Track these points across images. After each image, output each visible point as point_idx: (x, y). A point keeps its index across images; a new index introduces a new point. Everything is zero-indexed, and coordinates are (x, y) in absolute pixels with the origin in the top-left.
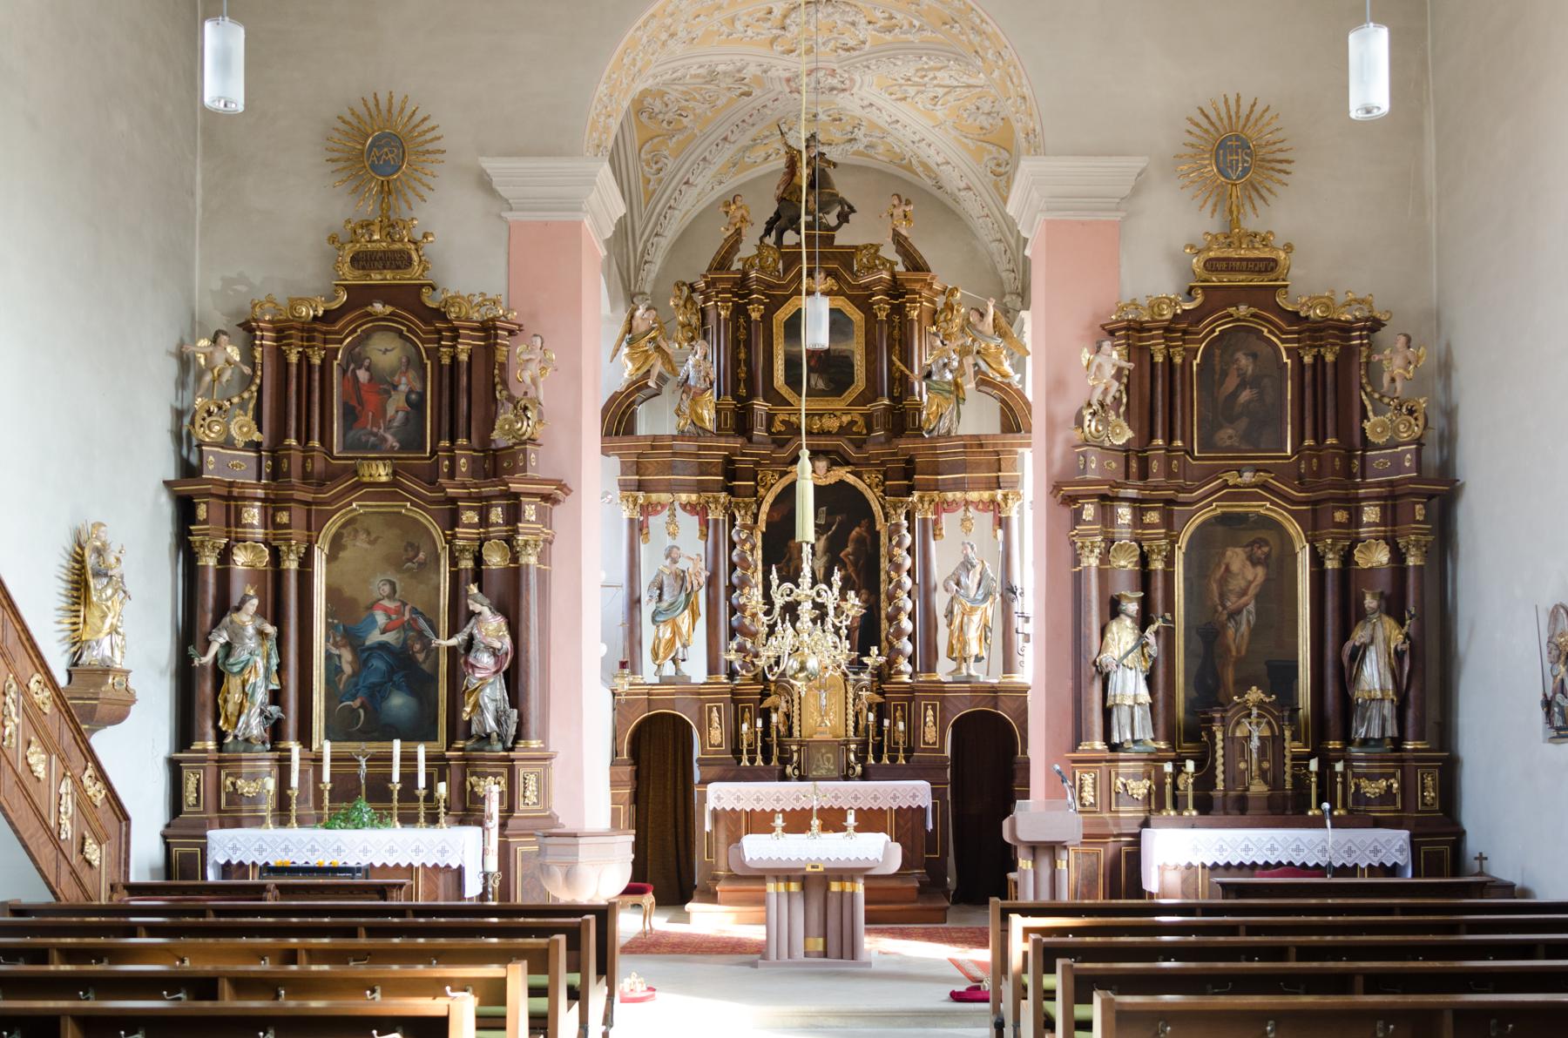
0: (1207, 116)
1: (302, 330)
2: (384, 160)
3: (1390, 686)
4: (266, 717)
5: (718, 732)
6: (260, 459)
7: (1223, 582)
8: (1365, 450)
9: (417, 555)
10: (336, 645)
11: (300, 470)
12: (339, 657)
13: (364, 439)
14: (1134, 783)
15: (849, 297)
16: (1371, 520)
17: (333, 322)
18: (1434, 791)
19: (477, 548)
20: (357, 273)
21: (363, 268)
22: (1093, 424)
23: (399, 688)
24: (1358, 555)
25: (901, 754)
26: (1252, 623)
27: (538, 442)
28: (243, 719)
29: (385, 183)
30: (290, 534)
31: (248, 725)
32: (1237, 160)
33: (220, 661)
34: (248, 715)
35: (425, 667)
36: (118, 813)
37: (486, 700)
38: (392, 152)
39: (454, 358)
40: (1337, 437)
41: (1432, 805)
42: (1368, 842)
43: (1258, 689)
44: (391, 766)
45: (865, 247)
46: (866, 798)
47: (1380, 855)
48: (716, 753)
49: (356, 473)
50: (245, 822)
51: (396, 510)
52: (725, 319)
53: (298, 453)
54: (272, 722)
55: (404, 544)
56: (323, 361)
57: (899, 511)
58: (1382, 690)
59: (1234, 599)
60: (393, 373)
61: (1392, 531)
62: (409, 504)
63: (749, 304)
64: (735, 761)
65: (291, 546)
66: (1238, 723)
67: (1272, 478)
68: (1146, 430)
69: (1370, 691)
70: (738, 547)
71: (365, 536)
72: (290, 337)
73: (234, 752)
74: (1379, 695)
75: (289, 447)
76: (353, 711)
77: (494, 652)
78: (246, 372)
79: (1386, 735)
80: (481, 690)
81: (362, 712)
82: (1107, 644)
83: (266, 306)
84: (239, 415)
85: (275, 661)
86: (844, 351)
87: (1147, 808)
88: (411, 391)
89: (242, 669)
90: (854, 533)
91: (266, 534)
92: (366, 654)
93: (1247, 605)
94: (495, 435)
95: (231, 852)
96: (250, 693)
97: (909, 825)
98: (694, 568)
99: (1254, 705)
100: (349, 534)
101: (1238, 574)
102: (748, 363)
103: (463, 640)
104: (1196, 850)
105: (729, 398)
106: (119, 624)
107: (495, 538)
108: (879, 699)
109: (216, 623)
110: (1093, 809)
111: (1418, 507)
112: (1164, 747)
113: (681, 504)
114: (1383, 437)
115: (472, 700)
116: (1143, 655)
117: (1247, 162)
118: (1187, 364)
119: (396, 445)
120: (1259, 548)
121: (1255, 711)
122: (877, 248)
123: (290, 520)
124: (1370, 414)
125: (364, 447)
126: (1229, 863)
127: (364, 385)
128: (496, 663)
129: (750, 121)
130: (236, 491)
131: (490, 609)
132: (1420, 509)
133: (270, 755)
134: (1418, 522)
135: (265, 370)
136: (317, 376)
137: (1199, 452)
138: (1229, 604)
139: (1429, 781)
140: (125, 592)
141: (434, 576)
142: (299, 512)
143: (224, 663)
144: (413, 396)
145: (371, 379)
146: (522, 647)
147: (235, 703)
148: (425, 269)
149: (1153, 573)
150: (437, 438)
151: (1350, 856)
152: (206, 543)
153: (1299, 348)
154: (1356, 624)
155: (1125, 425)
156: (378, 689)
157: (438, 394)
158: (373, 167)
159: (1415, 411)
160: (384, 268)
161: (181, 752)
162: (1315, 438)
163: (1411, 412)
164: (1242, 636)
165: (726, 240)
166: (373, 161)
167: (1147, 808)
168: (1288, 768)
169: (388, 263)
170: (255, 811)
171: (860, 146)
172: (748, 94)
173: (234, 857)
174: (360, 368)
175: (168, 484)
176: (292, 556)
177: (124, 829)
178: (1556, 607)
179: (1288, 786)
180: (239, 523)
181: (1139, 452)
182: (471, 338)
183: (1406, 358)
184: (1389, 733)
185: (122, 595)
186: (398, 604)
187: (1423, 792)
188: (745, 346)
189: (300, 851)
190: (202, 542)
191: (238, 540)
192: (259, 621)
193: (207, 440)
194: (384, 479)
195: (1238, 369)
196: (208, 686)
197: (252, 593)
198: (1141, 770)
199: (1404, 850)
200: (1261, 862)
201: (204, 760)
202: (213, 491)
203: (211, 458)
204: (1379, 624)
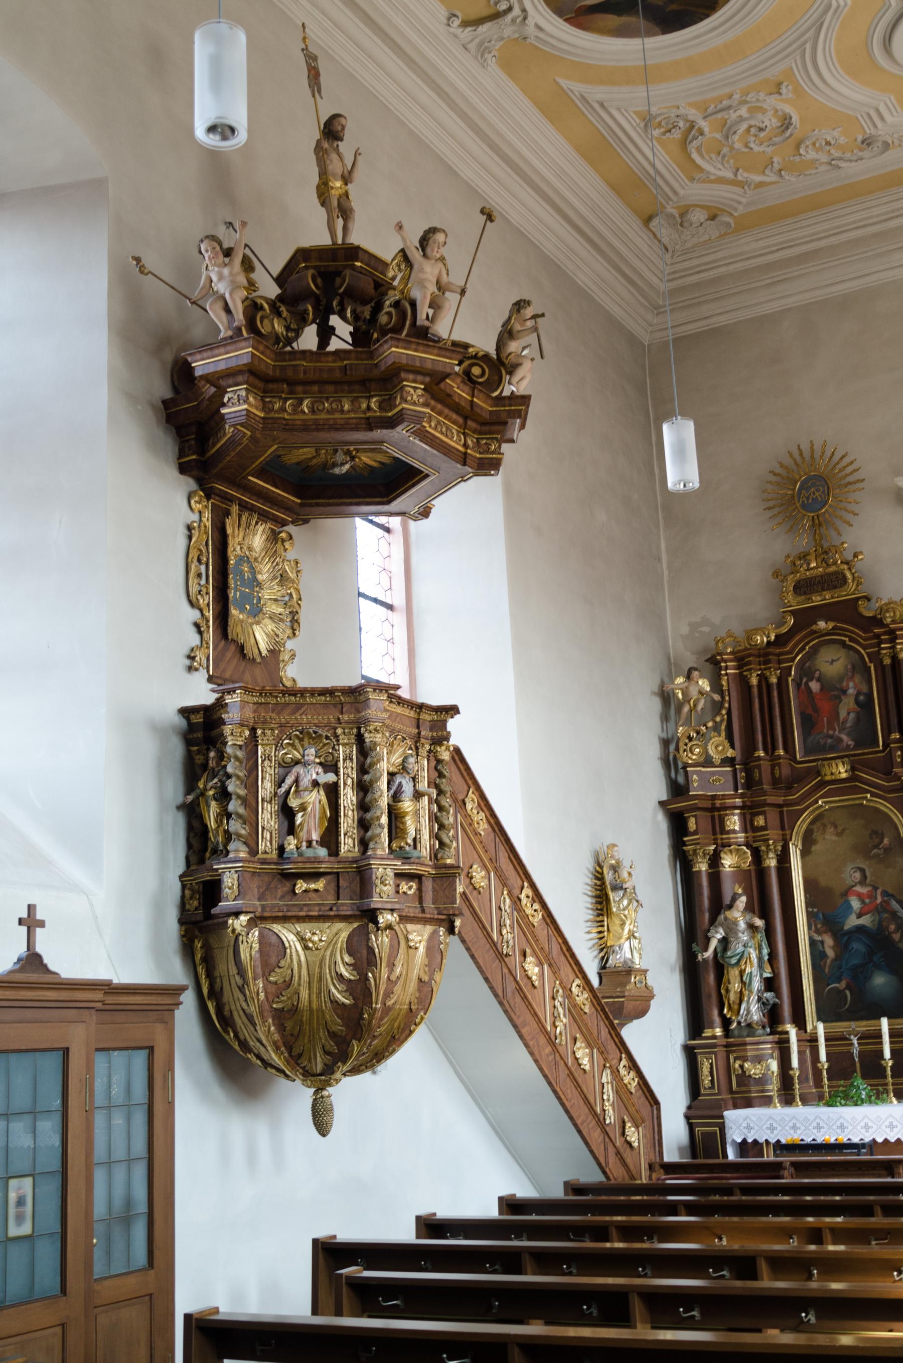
1: (759, 656)
6: (735, 772)
9: (882, 842)
10: (817, 932)
11: (770, 777)
12: (822, 942)
13: (822, 742)
17: (785, 644)
20: (800, 598)
21: (805, 593)
23: (878, 967)
28: (743, 1006)
29: (815, 517)
30: (768, 835)
31: (748, 1011)
38: (818, 490)
44: (881, 1043)
49: (818, 773)
51: (858, 802)
54: (769, 1007)
56: (779, 679)
60: (841, 680)
62: (869, 795)
71: (832, 829)
72: (749, 663)
73: (739, 1037)
76: (840, 992)
78: (716, 699)
81: (848, 993)
84: (714, 737)
85: (765, 951)
88: (859, 693)
89: (739, 961)
91: (747, 837)
92: (845, 939)
95: (746, 1131)
96: (747, 981)
106: (635, 929)
109: (713, 921)
119: (851, 743)
123: (766, 822)
125: (824, 749)
127: (816, 694)
130: (718, 803)
136: (775, 693)
140: (637, 901)
145: (822, 689)
147: (735, 992)
152: (698, 851)
158: (804, 506)
160: (823, 590)
161: (694, 1039)
166: (803, 502)
169: (826, 585)
174: (811, 680)
175: (662, 804)
176: (771, 855)
177: (655, 1112)
180: (723, 831)
190: (695, 850)
191: (724, 846)
192: (748, 916)
194: (844, 775)
196: (711, 978)
197: (740, 891)
201: (714, 1046)
203: (695, 777)
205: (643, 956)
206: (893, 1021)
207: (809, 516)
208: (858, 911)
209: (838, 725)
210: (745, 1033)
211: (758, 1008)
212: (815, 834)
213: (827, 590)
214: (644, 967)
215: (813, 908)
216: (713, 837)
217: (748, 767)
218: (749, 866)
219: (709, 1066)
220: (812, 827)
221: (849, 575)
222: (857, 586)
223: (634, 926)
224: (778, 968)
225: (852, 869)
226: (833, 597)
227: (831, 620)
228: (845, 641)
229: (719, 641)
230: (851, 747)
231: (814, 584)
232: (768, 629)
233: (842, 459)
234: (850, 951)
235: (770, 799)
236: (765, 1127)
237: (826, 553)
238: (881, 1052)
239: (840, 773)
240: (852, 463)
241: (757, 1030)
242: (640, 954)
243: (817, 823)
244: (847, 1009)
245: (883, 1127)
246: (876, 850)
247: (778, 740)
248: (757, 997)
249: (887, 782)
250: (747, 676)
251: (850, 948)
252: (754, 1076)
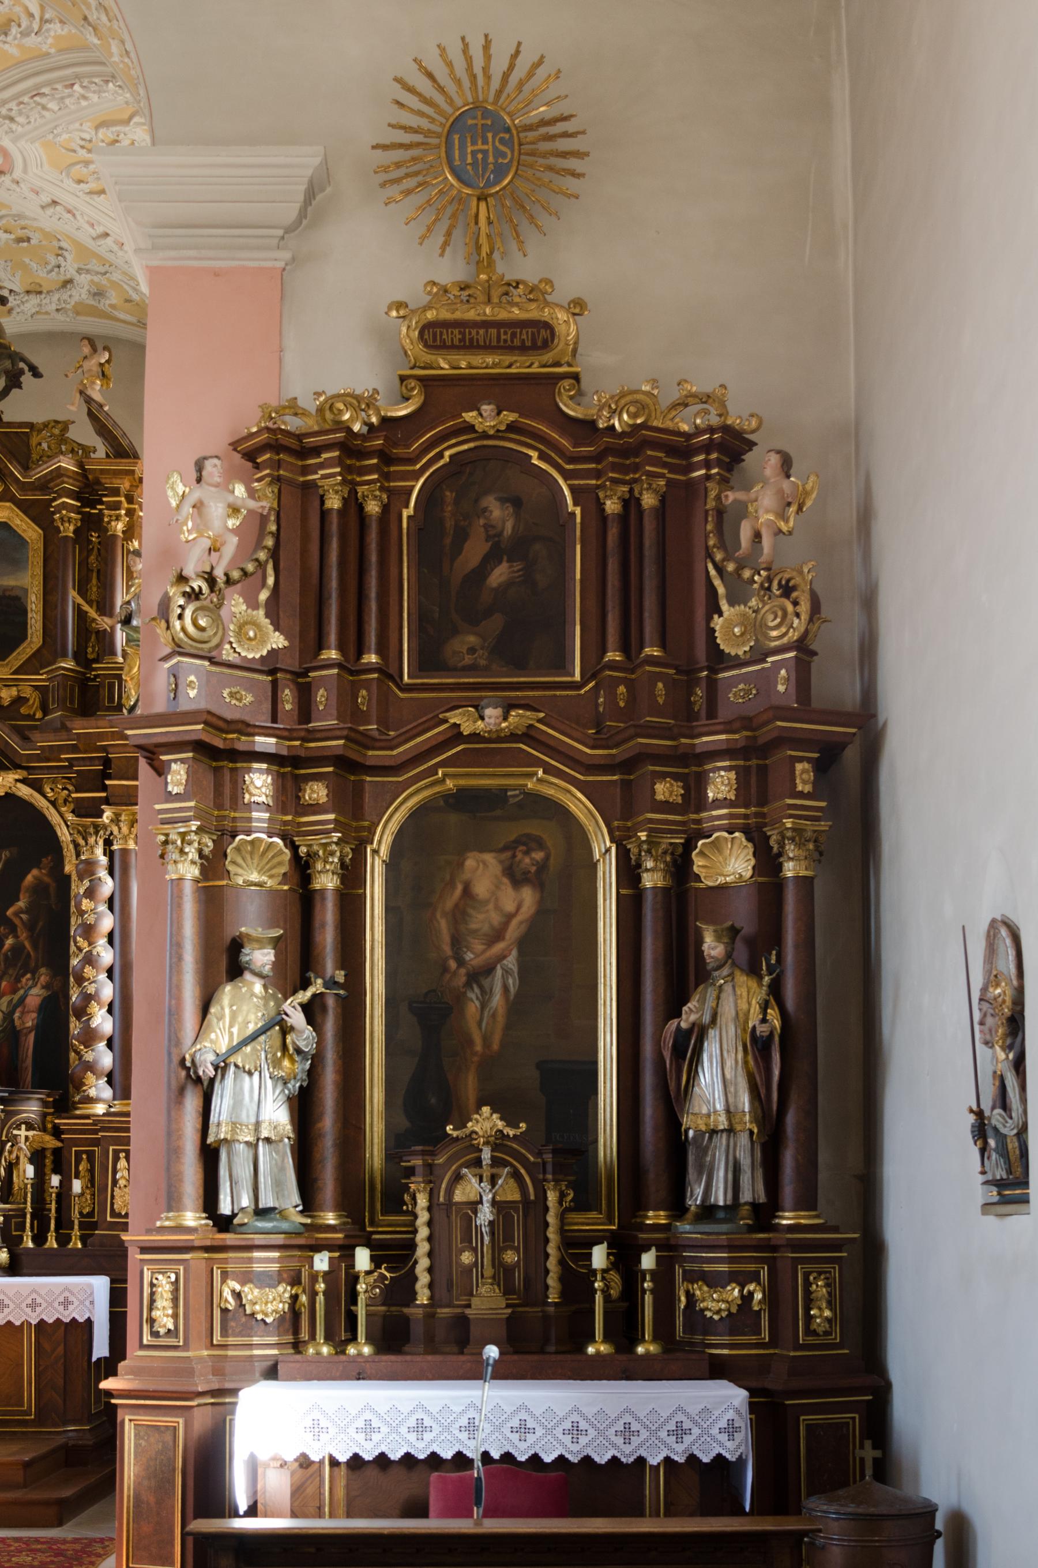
0: (430, 76)
3: (745, 1102)
7: (459, 915)
8: (713, 670)
14: (256, 1291)
15: (21, 505)
16: (720, 796)
18: (830, 1305)
22: (188, 613)
24: (698, 864)
25: (76, 1232)
26: (513, 990)
32: (485, 153)
40: (663, 645)
41: (827, 1333)
42: (665, 1415)
43: (494, 1111)
45: (46, 425)
46: (18, 1306)
47: (688, 1439)
57: (92, 840)
58: (728, 1111)
59: (480, 947)
61: (757, 815)
62: (540, 773)
66: (458, 1178)
67: (539, 721)
68: (312, 634)
69: (709, 1115)
74: (723, 1123)
79: (742, 1201)
82: (209, 1025)
86: (13, 588)
87: (289, 1338)
90: (29, 878)
93: (505, 957)
97: (61, 1349)
99: (486, 1143)
101: (487, 902)
104: (317, 1430)
108: (51, 1142)
110: (171, 1341)
111: (799, 767)
112: (332, 1222)
114: (744, 644)
116: (284, 1047)
117: (503, 155)
118: (393, 517)
120: (527, 853)
121: (486, 1155)
122: (65, 426)
124: (724, 606)
126: (382, 1456)
132: (803, 771)
134: (801, 795)
137: (409, 677)
138: (469, 956)
139: (820, 1288)
149: (317, 897)
151: (627, 1441)
153: (598, 487)
154: (697, 986)
155: (266, 622)
159: (794, 588)
162: (625, 648)
163: (787, 590)
164: (494, 1016)
167: (289, 1338)
168: (552, 1264)
171: (80, 294)
178: (994, 921)
179: (553, 1297)
181: (298, 675)
182: (665, 465)
183: (780, 492)
184: (746, 1196)
187: (807, 1309)
195: (486, 527)
198: (275, 1267)
199: (737, 1430)
200: (447, 1454)
204: (728, 988)
236: (612, 1431)
249: (592, 748)
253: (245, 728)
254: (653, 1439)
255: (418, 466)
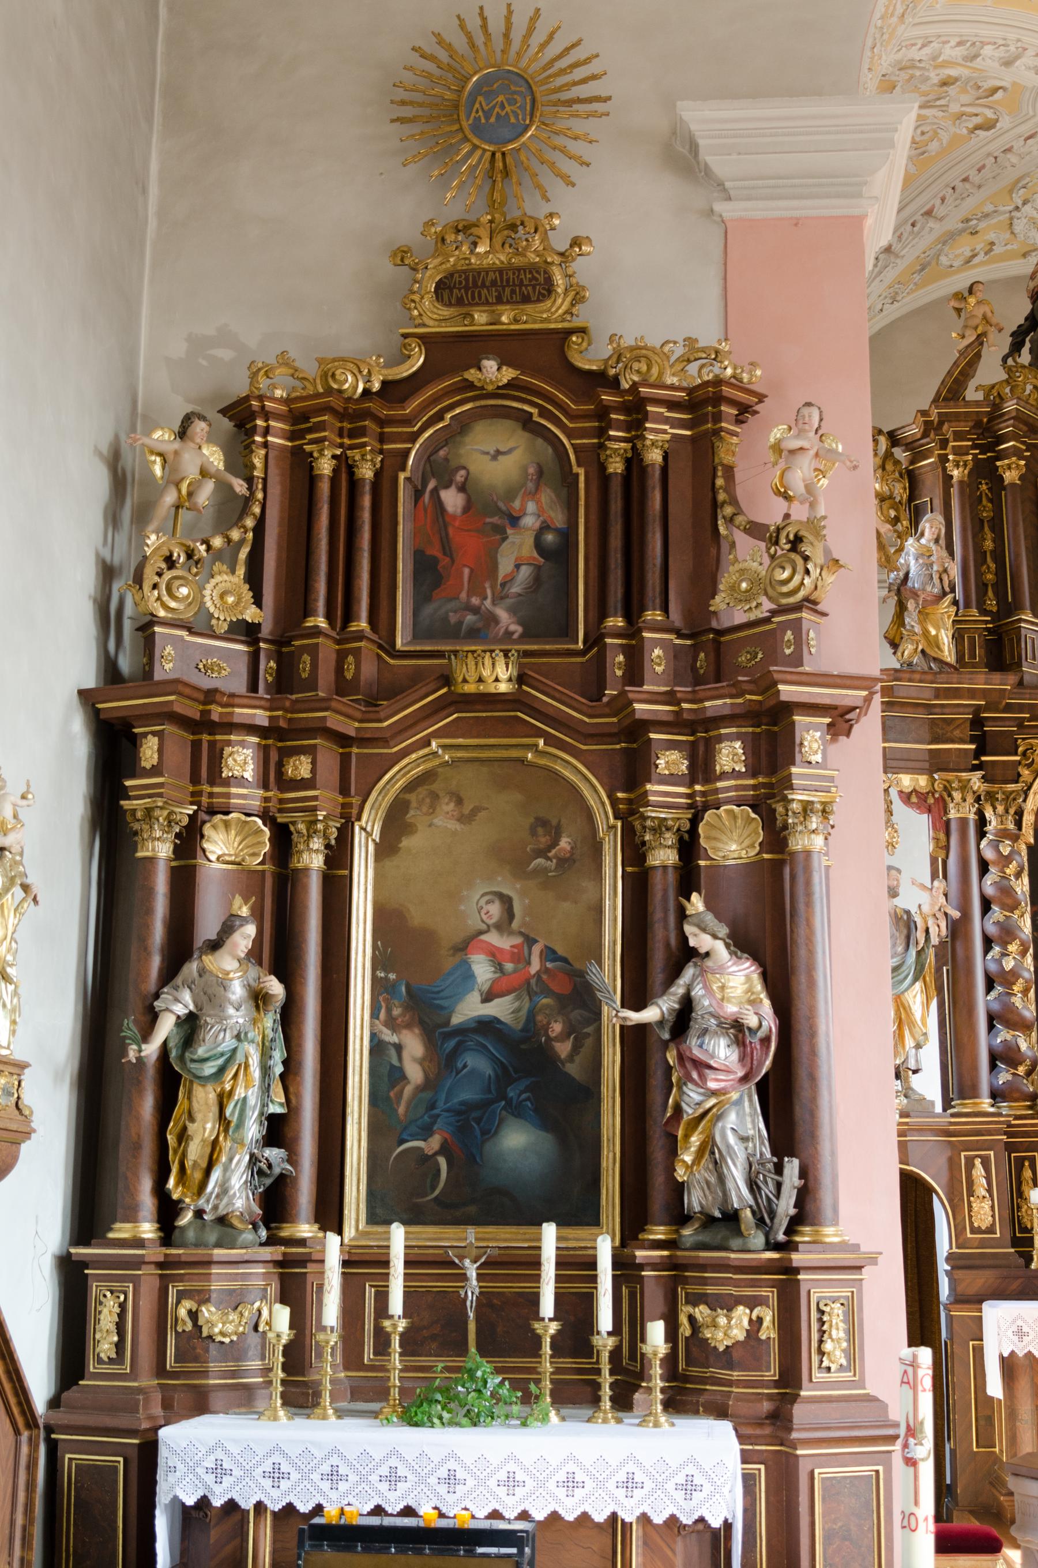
1: (341, 416)
2: (498, 115)
4: (261, 1173)
5: (986, 1205)
6: (254, 659)
9: (555, 843)
10: (392, 1024)
11: (332, 677)
12: (399, 1048)
13: (453, 618)
17: (403, 400)
19: (688, 826)
20: (446, 312)
21: (460, 302)
23: (516, 1111)
27: (819, 607)
28: (216, 1175)
29: (498, 156)
30: (315, 798)
31: (224, 1189)
33: (173, 1054)
34: (226, 1169)
35: (573, 1069)
36: (16, 1410)
37: (732, 1139)
38: (512, 102)
39: (634, 462)
44: (537, 1278)
48: (983, 1243)
49: (446, 679)
50: (216, 1399)
51: (514, 753)
52: (961, 482)
53: (330, 643)
54: (268, 1182)
55: (532, 820)
56: (378, 474)
60: (510, 494)
62: (541, 742)
63: (999, 458)
64: (1021, 1261)
65: (315, 822)
70: (992, 869)
71: (452, 805)
72: (320, 427)
73: (197, 1245)
75: (316, 632)
76: (425, 1160)
77: (738, 1030)
78: (238, 489)
80: (719, 1117)
81: (442, 1161)
83: (277, 372)
84: (220, 573)
85: (278, 1056)
88: (545, 528)
89: (222, 1070)
91: (266, 800)
92: (452, 1043)
94: (719, 602)
95: (210, 1479)
96: (235, 1120)
98: (932, 905)
100: (421, 803)
102: (998, 555)
103: (671, 1010)
105: (974, 611)
106: (9, 958)
107: (729, 801)
109: (170, 972)
113: (901, 792)
115: (695, 1140)
119: (517, 629)
123: (313, 771)
125: (454, 633)
127: (454, 517)
128: (742, 1059)
129: (976, 179)
130: (216, 712)
131: (727, 946)
133: (268, 1253)
135: (269, 491)
136: (366, 501)
140: (25, 888)
141: (588, 884)
142: (328, 756)
143: (181, 1058)
144: (550, 537)
145: (467, 508)
146: (801, 1025)
147: (203, 1140)
148: (578, 298)
150: (600, 610)
152: (157, 813)
156: (475, 1114)
157: (601, 534)
158: (476, 128)
160: (499, 301)
161: (87, 1244)
165: (962, 353)
166: (477, 119)
169: (508, 290)
170: (234, 1374)
172: (989, 125)
173: (218, 1489)
174: (447, 487)
175: (84, 695)
176: (317, 843)
177: (25, 1449)
180: (215, 776)
182: (666, 421)
185: (19, 893)
186: (518, 940)
188: (993, 530)
189: (363, 1479)
190: (149, 812)
191: (212, 812)
192: (253, 971)
193: (162, 613)
194: (503, 687)
196: (147, 1105)
197: (245, 911)
201: (137, 1263)
202: (178, 709)
203: (169, 649)
205: (19, 1029)
206: (570, 1232)
207: (485, 150)
208: (486, 987)
209: (493, 588)
210: (212, 1237)
211: (246, 1182)
212: (412, 813)
213: (508, 302)
214: (18, 1056)
215: (387, 972)
216: (191, 789)
217: (284, 650)
218: (262, 863)
219: (117, 1310)
220: (407, 796)
221: (559, 280)
222: (573, 305)
223: (9, 951)
224: (299, 1096)
225: (483, 895)
226: (516, 321)
227: (510, 365)
228: (531, 414)
229: (259, 370)
230: (515, 636)
231: (483, 285)
232: (369, 364)
233: (567, 50)
234: (457, 1073)
235: (335, 721)
236: (260, 1470)
237: (513, 227)
238: (534, 1300)
239: (497, 680)
240: (587, 61)
241: (241, 1232)
242: (14, 1022)
243: (420, 789)
244: (436, 1198)
245: (551, 1485)
246: (540, 861)
247: (359, 602)
248: (247, 1157)
249: (590, 716)
250: (311, 454)
251: (460, 1065)
252: (219, 1338)
253: (232, 700)
254: (248, 1480)
255: (415, 429)
